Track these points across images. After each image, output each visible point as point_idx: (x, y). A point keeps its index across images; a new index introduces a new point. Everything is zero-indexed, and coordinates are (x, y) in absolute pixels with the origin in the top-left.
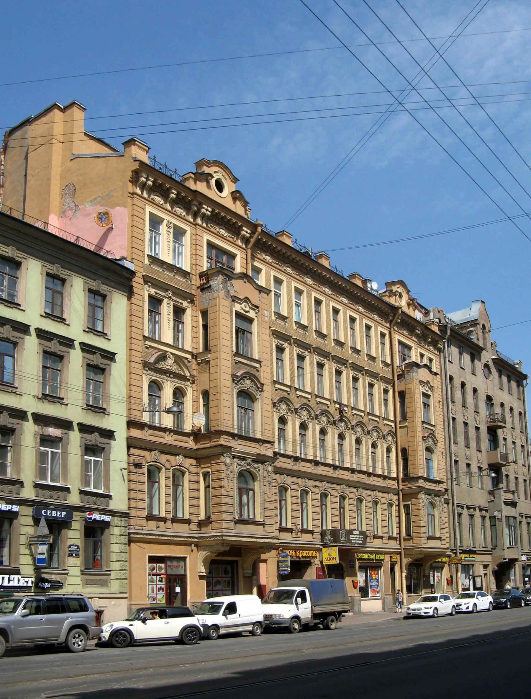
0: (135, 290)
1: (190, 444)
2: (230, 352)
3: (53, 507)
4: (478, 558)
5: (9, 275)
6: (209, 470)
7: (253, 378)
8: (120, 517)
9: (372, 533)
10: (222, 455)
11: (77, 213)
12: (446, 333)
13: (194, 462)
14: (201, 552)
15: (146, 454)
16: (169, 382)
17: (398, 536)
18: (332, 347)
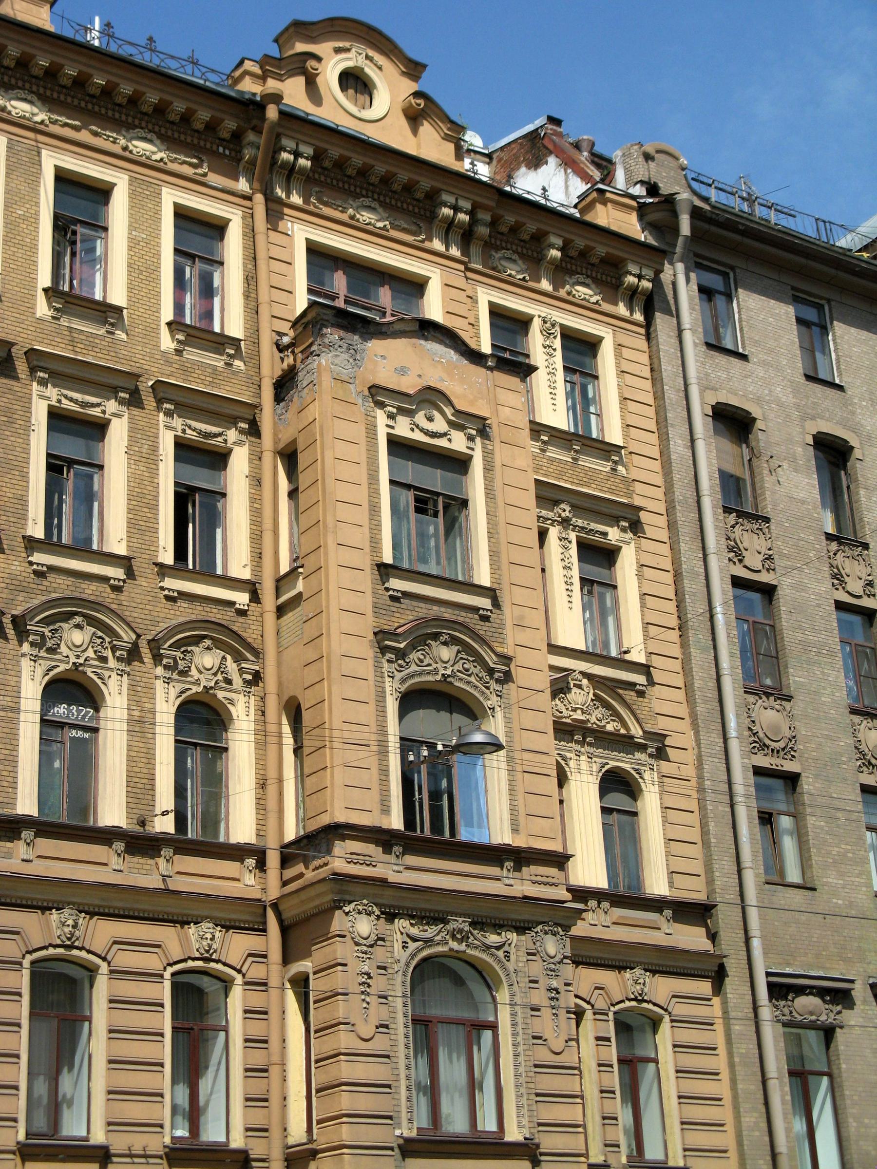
12: (676, 230)
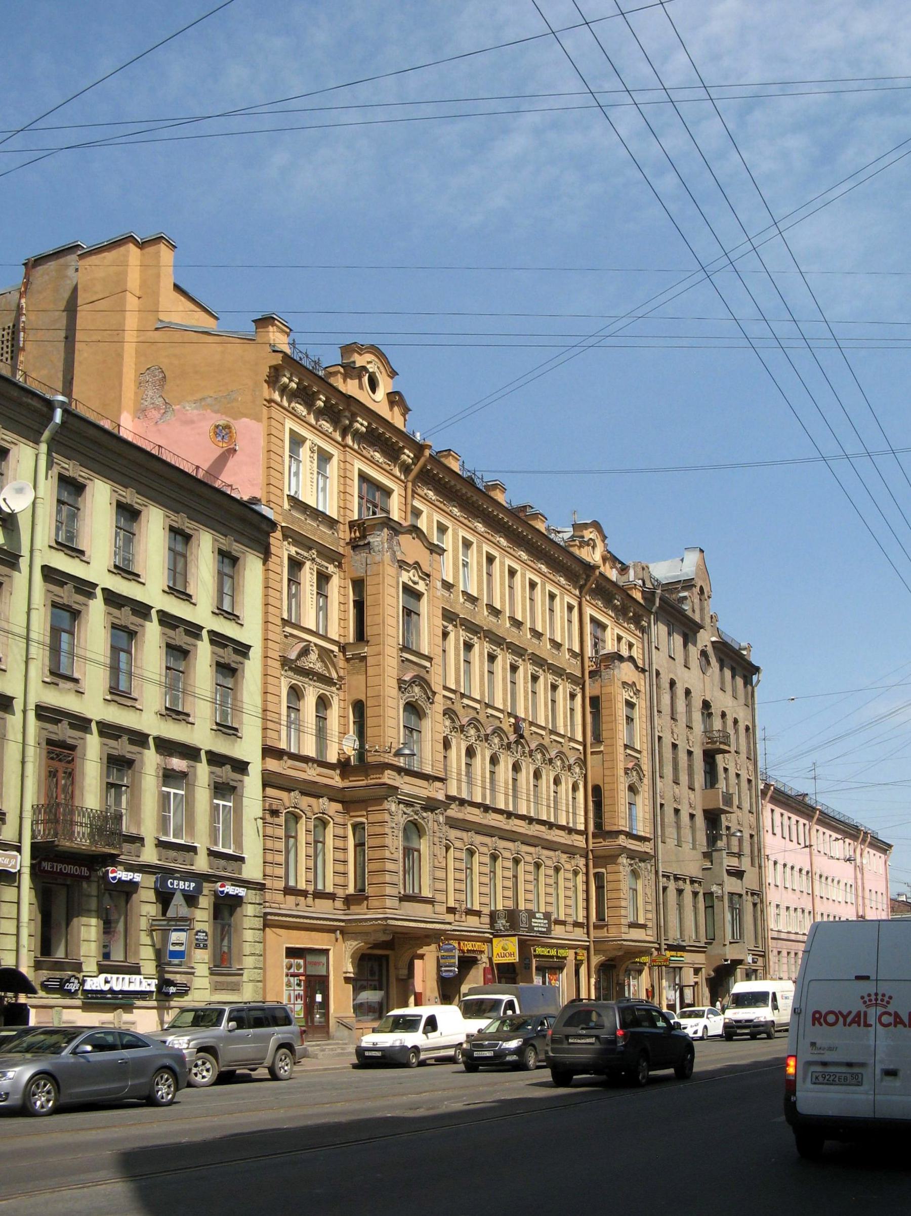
0: (273, 550)
1: (335, 780)
2: (395, 645)
3: (178, 875)
4: (688, 957)
5: (124, 530)
6: (363, 820)
7: (422, 682)
8: (254, 889)
9: (464, 907)
10: (387, 799)
11: (168, 416)
12: (654, 604)
13: (339, 806)
14: (349, 943)
15: (283, 795)
16: (311, 688)
17: (585, 921)
18: (507, 630)
